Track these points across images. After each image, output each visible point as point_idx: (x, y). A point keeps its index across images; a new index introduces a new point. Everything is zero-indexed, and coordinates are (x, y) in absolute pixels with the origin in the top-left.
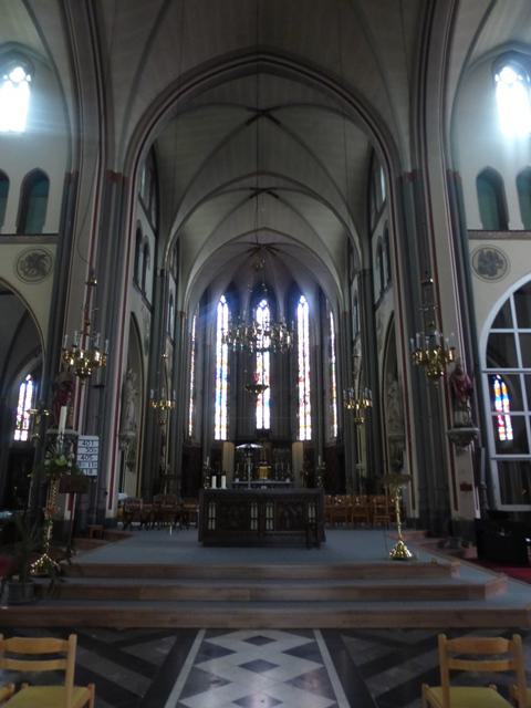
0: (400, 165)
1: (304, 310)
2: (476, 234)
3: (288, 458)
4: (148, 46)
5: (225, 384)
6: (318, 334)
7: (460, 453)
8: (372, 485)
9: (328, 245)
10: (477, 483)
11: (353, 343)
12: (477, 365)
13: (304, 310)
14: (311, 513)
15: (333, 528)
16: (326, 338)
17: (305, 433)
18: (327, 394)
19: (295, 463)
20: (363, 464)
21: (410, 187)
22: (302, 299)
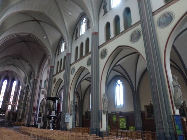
0: (35, 78)
1: (15, 84)
2: (42, 88)
6: (17, 89)
7: (33, 117)
8: (21, 121)
9: (23, 76)
10: (34, 120)
11: (23, 95)
12: (38, 105)
13: (15, 84)
14: (12, 124)
16: (18, 91)
17: (10, 108)
18: (17, 97)
20: (20, 117)
21: (35, 80)
22: (15, 81)
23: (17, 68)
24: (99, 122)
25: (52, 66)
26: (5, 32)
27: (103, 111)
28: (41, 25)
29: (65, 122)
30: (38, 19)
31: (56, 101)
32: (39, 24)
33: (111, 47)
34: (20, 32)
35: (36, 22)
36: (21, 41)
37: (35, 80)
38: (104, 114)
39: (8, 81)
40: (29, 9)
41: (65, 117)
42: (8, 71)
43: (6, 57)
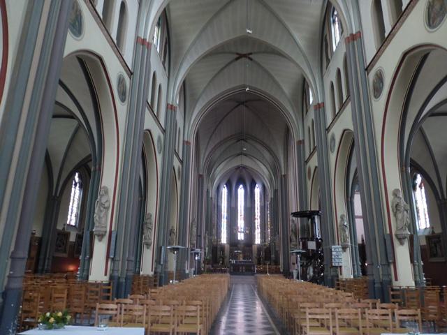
1: (258, 191)
3: (251, 251)
4: (210, 139)
5: (226, 220)
15: (220, 241)
17: (258, 241)
19: (253, 252)
21: (283, 178)
22: (257, 185)
23: (250, 158)
24: (389, 264)
25: (300, 141)
26: (199, 99)
27: (396, 235)
28: (256, 60)
29: (333, 265)
30: (244, 52)
31: (314, 218)
32: (251, 59)
33: (389, 63)
34: (224, 89)
35: (243, 59)
36: (237, 104)
37: (283, 178)
38: (402, 244)
39: (245, 187)
40: (219, 42)
41: (331, 255)
42: (238, 168)
43: (221, 143)
